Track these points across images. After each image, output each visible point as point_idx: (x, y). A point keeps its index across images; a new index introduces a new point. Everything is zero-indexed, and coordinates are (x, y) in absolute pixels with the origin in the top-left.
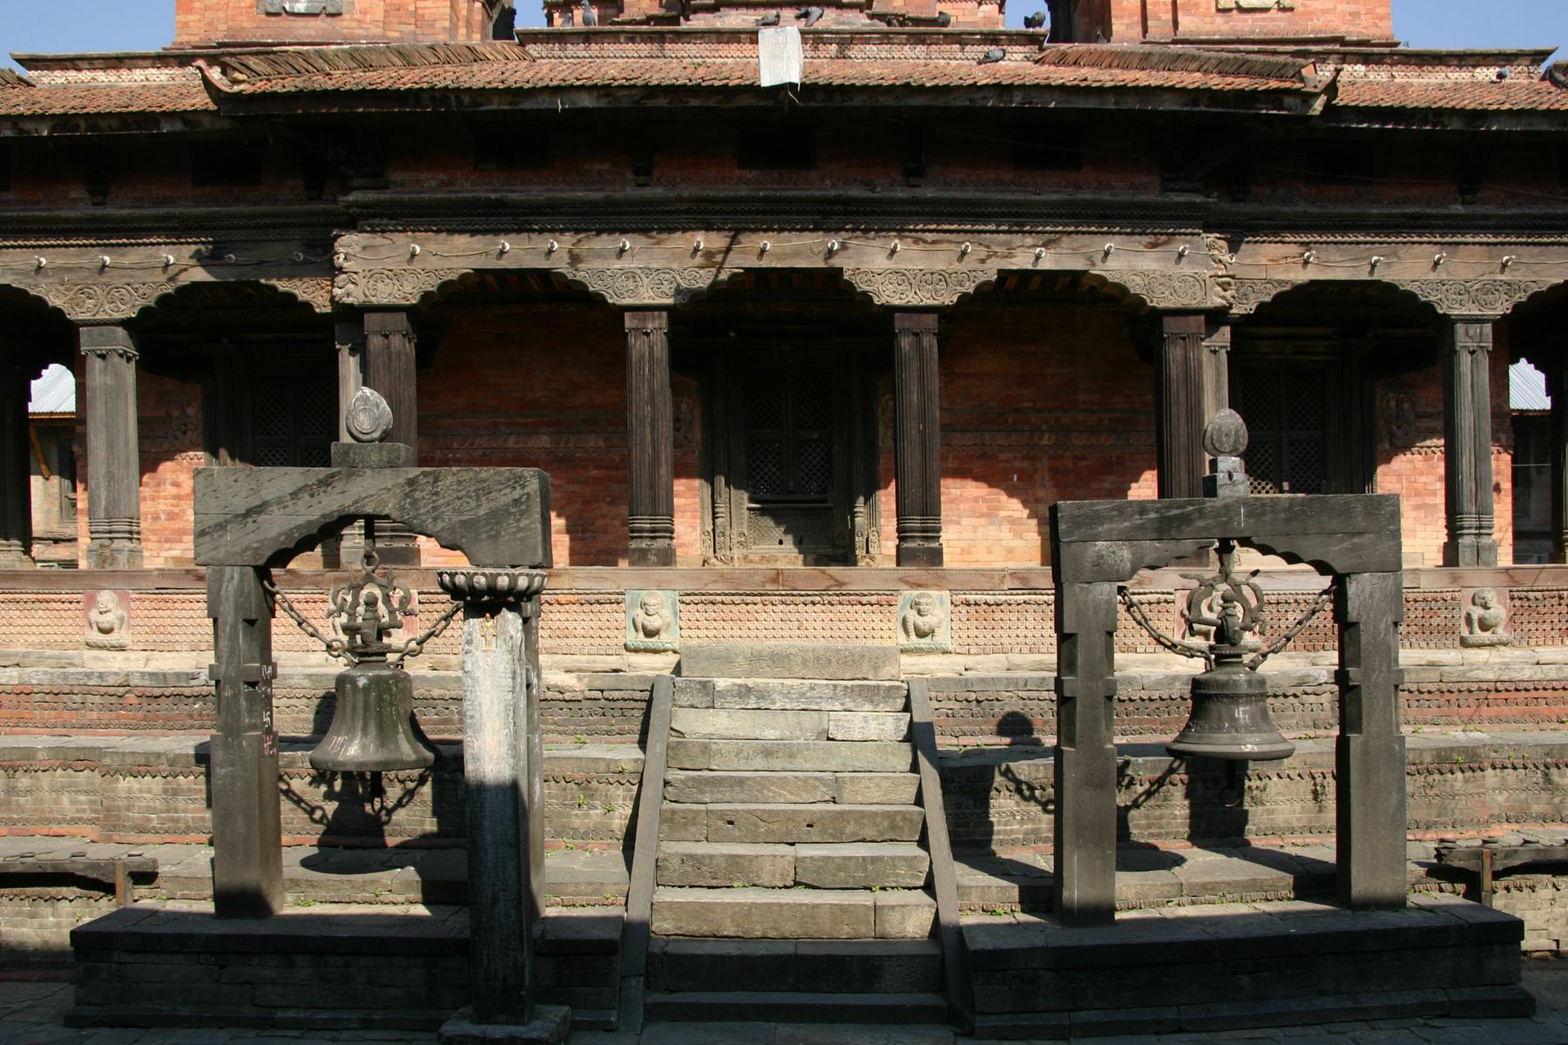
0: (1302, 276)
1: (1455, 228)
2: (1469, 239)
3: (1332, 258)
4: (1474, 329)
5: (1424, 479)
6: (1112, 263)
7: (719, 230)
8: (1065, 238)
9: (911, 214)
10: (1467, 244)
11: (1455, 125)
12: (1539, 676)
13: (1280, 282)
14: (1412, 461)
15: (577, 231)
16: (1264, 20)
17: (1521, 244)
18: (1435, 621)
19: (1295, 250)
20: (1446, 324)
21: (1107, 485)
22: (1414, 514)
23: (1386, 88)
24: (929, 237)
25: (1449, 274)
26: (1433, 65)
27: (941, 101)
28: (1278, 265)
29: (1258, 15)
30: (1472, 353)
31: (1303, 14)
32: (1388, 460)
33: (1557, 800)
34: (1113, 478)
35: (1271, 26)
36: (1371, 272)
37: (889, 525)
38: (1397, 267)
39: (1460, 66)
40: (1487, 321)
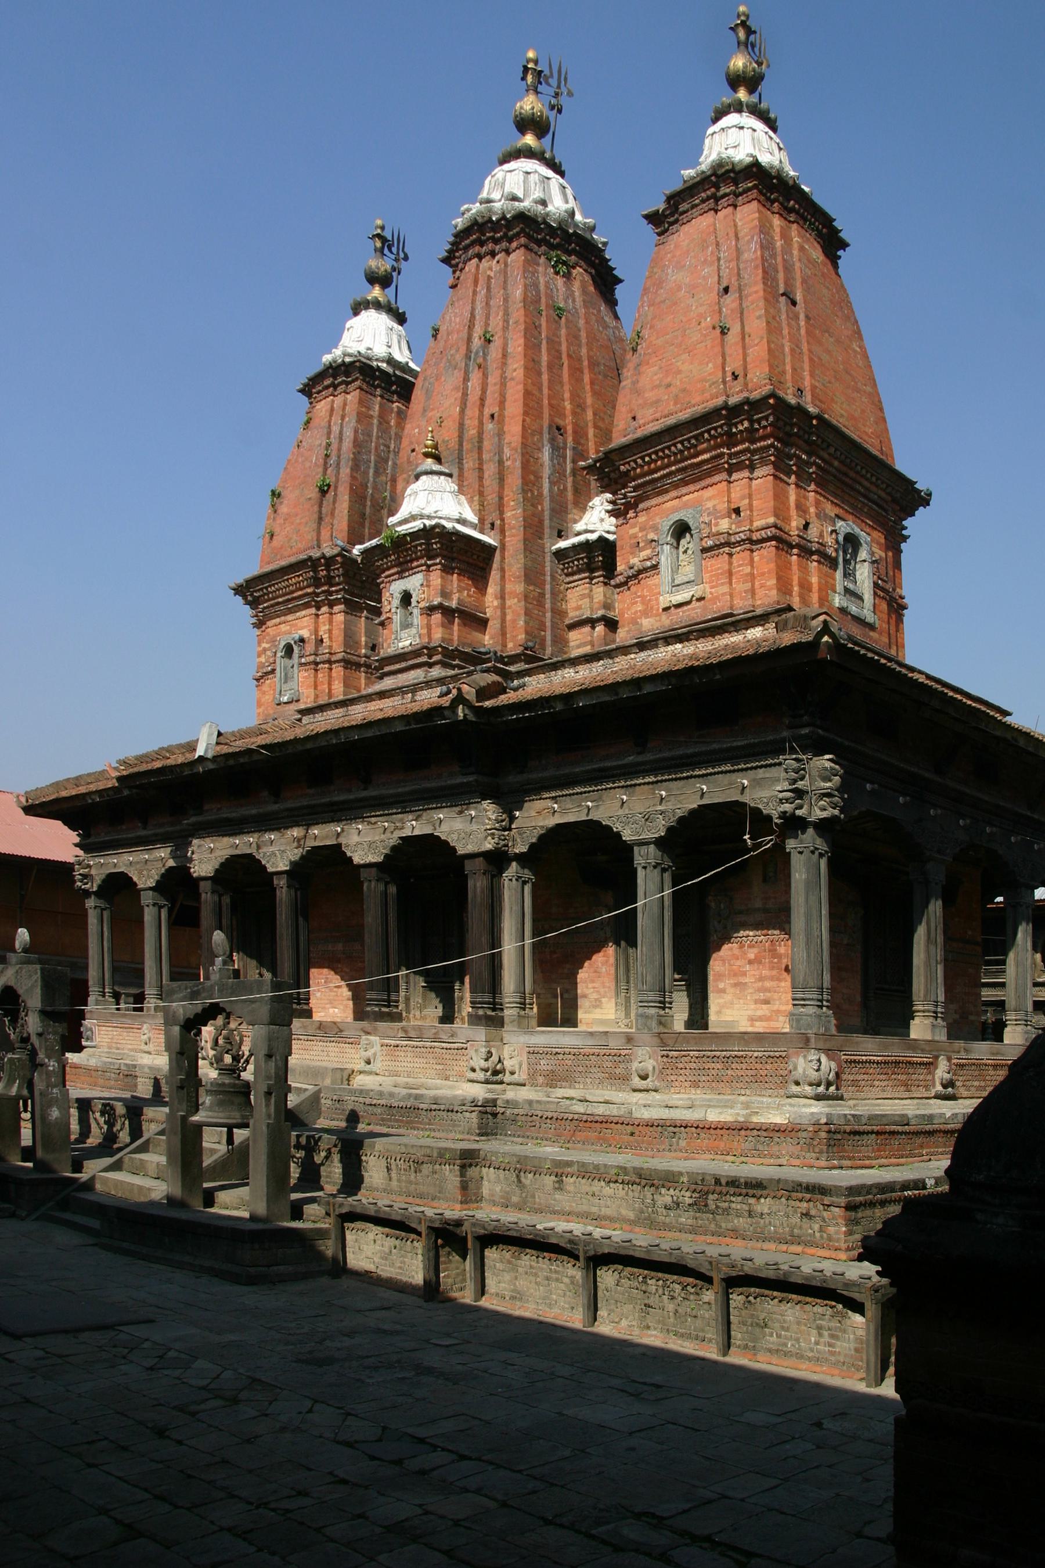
0: (552, 821)
1: (719, 760)
2: (641, 781)
3: (567, 806)
4: (644, 849)
5: (739, 963)
6: (445, 827)
7: (299, 826)
8: (425, 814)
9: (364, 807)
10: (639, 785)
11: (559, 707)
12: (608, 1113)
13: (542, 827)
14: (731, 949)
15: (259, 831)
16: (688, 610)
17: (669, 780)
18: (618, 1071)
19: (549, 803)
20: (627, 849)
21: (566, 971)
22: (732, 990)
23: (691, 657)
24: (373, 820)
25: (630, 809)
26: (720, 634)
27: (385, 730)
28: (541, 815)
29: (685, 608)
30: (645, 868)
31: (710, 600)
32: (719, 949)
33: (524, 1195)
34: (568, 966)
35: (693, 614)
36: (588, 815)
37: (468, 995)
38: (602, 808)
39: (737, 631)
40: (647, 844)
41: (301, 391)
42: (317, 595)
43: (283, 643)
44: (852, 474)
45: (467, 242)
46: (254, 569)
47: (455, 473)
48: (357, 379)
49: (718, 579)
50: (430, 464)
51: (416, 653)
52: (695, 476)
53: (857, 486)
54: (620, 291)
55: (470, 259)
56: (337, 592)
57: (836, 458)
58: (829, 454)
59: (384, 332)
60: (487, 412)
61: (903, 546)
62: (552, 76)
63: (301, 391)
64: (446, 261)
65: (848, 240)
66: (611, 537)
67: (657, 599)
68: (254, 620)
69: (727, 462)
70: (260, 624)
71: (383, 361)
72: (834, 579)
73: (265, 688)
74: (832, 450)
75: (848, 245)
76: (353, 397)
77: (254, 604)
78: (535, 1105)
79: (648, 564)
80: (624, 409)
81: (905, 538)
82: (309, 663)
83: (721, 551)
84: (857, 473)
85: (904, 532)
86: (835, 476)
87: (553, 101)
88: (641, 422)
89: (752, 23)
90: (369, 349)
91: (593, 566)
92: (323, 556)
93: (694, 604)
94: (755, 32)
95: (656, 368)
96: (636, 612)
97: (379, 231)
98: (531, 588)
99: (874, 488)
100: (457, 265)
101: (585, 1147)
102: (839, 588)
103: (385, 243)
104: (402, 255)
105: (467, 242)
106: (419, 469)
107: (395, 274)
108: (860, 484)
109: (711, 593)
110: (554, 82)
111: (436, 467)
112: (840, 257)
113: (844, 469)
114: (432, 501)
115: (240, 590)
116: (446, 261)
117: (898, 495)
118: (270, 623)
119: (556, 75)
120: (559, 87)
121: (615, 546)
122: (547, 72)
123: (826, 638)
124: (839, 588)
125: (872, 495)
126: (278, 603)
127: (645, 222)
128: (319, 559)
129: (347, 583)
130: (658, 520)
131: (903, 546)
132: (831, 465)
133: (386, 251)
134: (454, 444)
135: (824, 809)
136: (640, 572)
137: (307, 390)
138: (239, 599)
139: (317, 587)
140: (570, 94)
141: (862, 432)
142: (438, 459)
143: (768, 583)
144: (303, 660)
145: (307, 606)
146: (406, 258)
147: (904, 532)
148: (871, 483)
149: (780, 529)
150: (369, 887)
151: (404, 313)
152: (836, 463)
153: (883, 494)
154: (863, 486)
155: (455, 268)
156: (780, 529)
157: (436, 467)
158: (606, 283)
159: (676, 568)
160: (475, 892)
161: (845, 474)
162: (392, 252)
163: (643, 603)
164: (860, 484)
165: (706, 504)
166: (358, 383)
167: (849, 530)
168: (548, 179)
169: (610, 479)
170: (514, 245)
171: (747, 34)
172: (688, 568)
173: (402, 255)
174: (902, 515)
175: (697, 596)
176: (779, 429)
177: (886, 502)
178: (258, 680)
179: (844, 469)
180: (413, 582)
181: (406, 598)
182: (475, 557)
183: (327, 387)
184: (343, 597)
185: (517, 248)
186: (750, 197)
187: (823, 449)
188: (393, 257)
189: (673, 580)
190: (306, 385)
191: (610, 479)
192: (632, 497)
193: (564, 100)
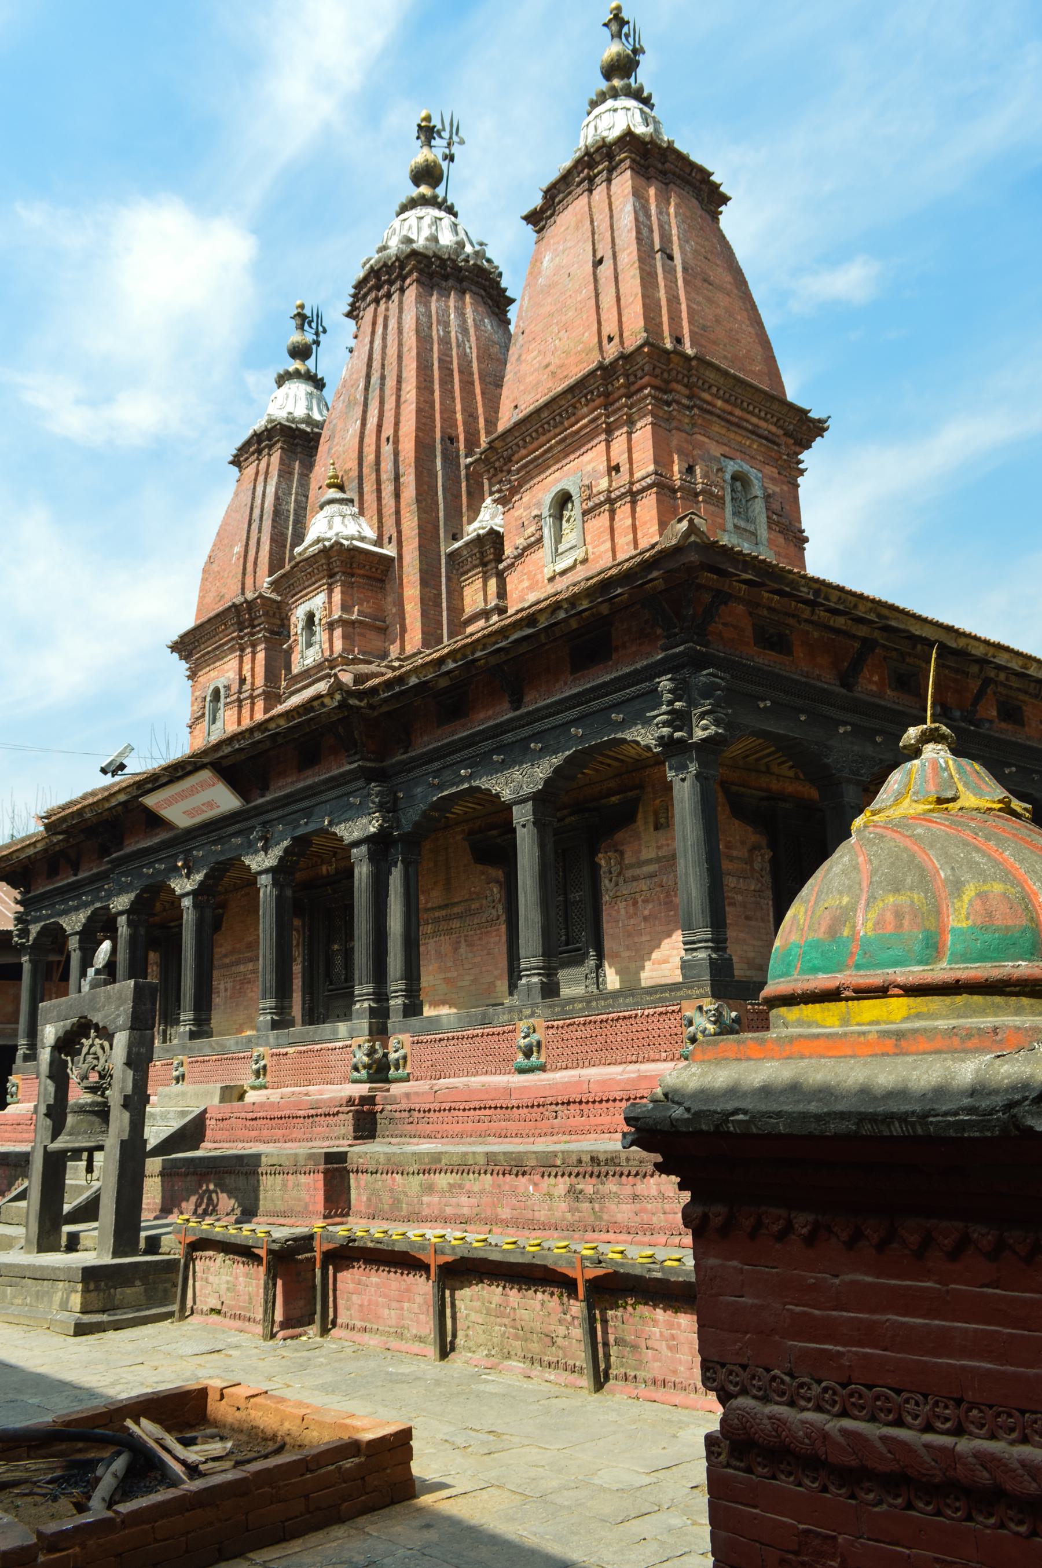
41: (232, 463)
42: (241, 638)
43: (211, 688)
44: (738, 412)
45: (365, 290)
46: (187, 621)
47: (356, 499)
48: (278, 441)
49: (599, 538)
50: (333, 493)
51: (319, 667)
52: (574, 445)
53: (745, 424)
54: (513, 312)
55: (369, 305)
56: (259, 632)
57: (719, 398)
58: (711, 394)
59: (303, 397)
60: (384, 436)
61: (800, 480)
62: (444, 129)
63: (232, 463)
64: (349, 315)
65: (729, 193)
66: (501, 530)
67: (542, 572)
68: (188, 673)
69: (605, 422)
70: (193, 675)
71: (302, 422)
72: (724, 518)
73: (196, 733)
74: (714, 390)
75: (728, 199)
76: (276, 457)
77: (186, 658)
78: (414, 1099)
79: (533, 539)
80: (507, 402)
81: (802, 472)
82: (234, 702)
83: (602, 509)
84: (743, 410)
85: (801, 466)
86: (719, 417)
87: (447, 151)
88: (523, 407)
89: (625, 15)
90: (290, 413)
91: (486, 559)
92: (246, 601)
93: (579, 567)
94: (628, 22)
95: (535, 353)
96: (523, 589)
97: (300, 310)
98: (428, 589)
99: (762, 424)
100: (358, 315)
101: (463, 1140)
102: (729, 526)
103: (302, 319)
104: (321, 329)
105: (365, 290)
106: (323, 499)
107: (314, 347)
108: (747, 421)
109: (593, 553)
110: (446, 135)
111: (340, 495)
112: (721, 213)
113: (729, 408)
114: (330, 525)
115: (176, 647)
116: (349, 315)
117: (791, 427)
118: (200, 673)
119: (448, 128)
120: (451, 138)
121: (503, 537)
122: (439, 127)
123: (693, 538)
124: (729, 526)
125: (760, 431)
126: (208, 653)
127: (525, 223)
128: (242, 604)
129: (268, 623)
130: (540, 495)
131: (800, 480)
132: (714, 406)
133: (306, 327)
134: (355, 473)
135: (705, 728)
136: (525, 549)
137: (237, 461)
138: (176, 655)
139: (241, 630)
140: (462, 142)
141: (753, 375)
142: (341, 488)
143: (651, 531)
144: (228, 700)
145: (232, 650)
146: (325, 331)
147: (801, 466)
148: (760, 418)
149: (661, 475)
150: (265, 893)
151: (322, 379)
152: (719, 403)
153: (773, 429)
154: (751, 424)
155: (356, 318)
156: (661, 475)
157: (340, 495)
158: (495, 300)
159: (558, 538)
160: (360, 879)
161: (731, 413)
162: (311, 327)
163: (529, 579)
164: (747, 421)
165: (584, 470)
166: (279, 445)
167: (737, 468)
168: (441, 219)
169: (496, 469)
170: (408, 281)
171: (618, 22)
172: (570, 535)
173: (321, 329)
174: (797, 449)
175: (580, 559)
176: (656, 377)
177: (778, 436)
178: (190, 727)
179: (729, 408)
180: (317, 602)
181: (310, 617)
182: (374, 570)
183: (253, 453)
184: (264, 636)
185: (410, 285)
186: (624, 168)
187: (704, 391)
188: (313, 331)
189: (557, 549)
190: (235, 456)
191: (496, 469)
192: (516, 480)
193: (455, 149)
